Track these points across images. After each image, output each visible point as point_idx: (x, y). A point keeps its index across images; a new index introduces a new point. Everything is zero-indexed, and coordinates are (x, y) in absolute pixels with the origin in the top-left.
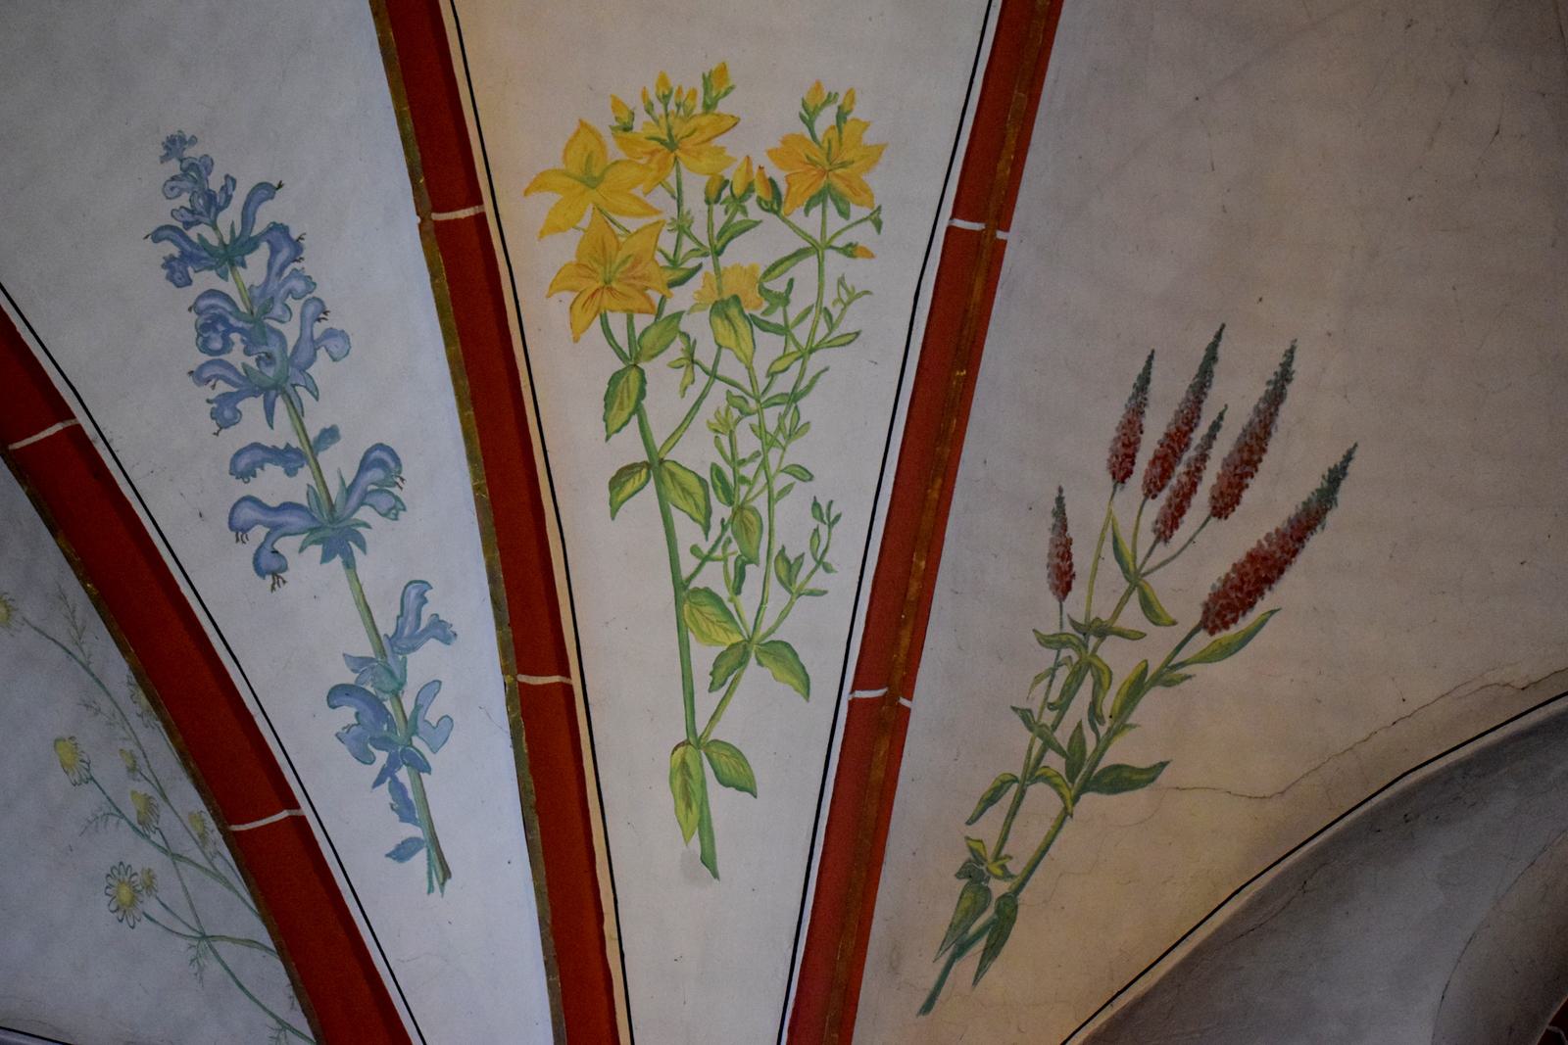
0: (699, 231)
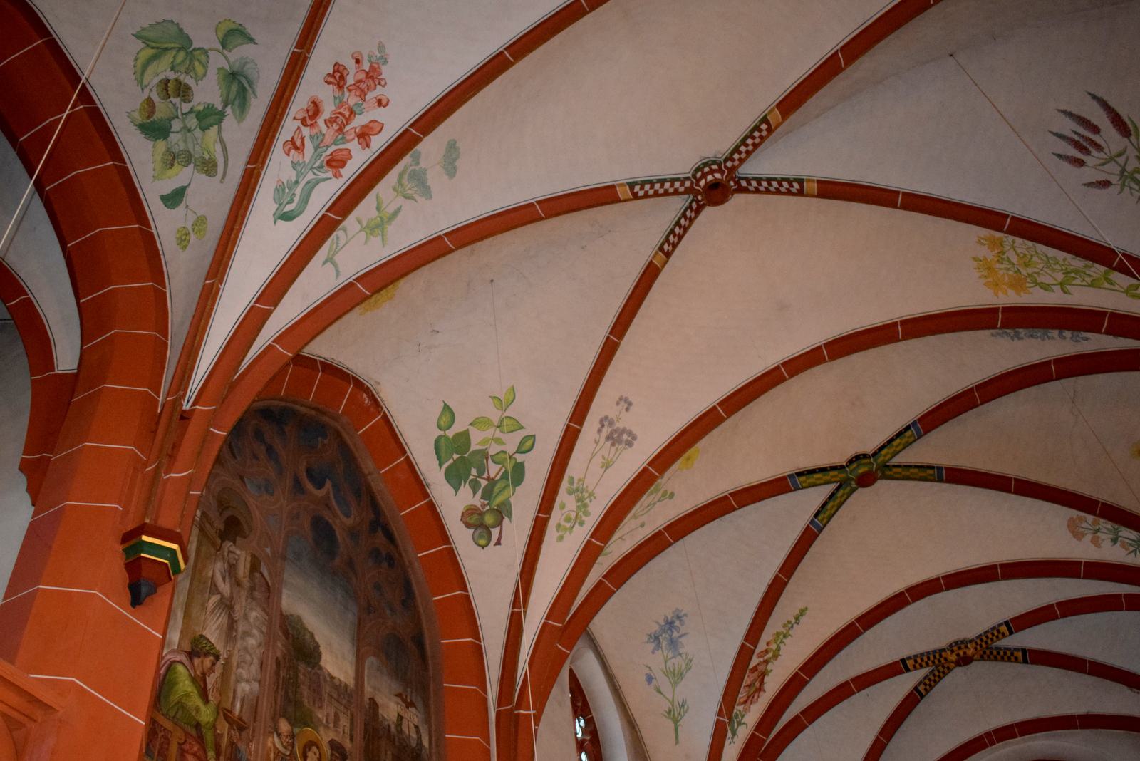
0: (1009, 266)
